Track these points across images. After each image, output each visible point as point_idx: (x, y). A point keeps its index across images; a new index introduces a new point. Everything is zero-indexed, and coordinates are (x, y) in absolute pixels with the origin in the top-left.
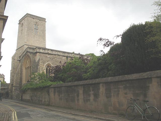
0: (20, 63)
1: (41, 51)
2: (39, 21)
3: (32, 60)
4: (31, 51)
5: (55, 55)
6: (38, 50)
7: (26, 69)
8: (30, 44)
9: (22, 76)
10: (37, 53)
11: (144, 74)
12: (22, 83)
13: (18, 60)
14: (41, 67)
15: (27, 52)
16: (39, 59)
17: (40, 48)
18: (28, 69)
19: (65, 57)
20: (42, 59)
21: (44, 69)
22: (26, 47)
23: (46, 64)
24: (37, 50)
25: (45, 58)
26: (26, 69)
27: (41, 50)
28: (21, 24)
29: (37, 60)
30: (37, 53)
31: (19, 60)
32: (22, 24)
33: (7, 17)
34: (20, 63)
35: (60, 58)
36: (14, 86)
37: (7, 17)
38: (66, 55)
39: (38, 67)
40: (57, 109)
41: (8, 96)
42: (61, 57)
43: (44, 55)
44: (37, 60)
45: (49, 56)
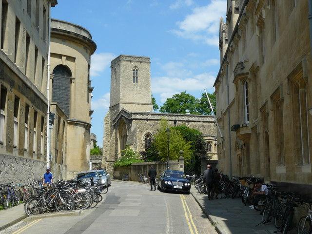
1: (138, 117)
5: (158, 120)
6: (133, 117)
10: (132, 120)
12: (117, 157)
15: (122, 116)
16: (136, 128)
21: (142, 139)
23: (145, 133)
30: (132, 120)
45: (148, 122)
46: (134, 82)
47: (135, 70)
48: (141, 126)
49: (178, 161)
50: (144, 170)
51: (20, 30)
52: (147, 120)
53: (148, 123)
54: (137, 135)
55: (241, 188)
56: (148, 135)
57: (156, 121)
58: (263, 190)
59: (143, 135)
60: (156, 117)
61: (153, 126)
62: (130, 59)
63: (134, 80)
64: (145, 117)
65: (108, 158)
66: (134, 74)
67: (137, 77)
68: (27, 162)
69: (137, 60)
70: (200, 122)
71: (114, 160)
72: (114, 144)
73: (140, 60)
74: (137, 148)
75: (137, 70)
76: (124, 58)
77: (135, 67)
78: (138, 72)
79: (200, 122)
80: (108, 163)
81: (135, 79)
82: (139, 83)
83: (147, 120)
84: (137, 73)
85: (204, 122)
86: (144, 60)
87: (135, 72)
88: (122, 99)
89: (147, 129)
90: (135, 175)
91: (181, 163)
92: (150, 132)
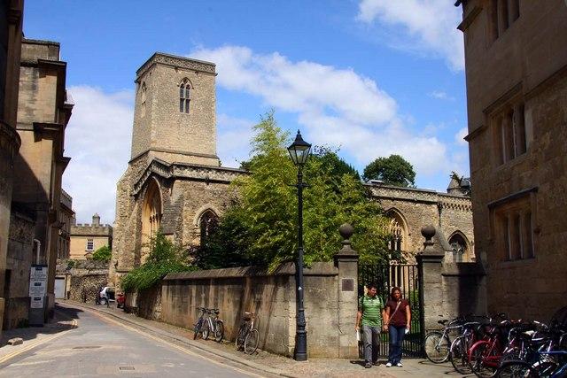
1: (187, 173)
4: (161, 172)
6: (177, 173)
10: (173, 179)
12: (139, 261)
14: (185, 220)
15: (153, 173)
16: (181, 198)
21: (194, 223)
29: (174, 200)
30: (173, 179)
36: (118, 267)
39: (177, 220)
43: (196, 183)
45: (210, 187)
47: (185, 85)
49: (336, 265)
50: (198, 294)
52: (208, 181)
53: (208, 188)
54: (184, 214)
55: (537, 364)
56: (207, 214)
59: (197, 215)
60: (226, 177)
62: (177, 63)
64: (203, 174)
65: (120, 264)
66: (182, 95)
67: (188, 101)
68: (40, 285)
73: (196, 67)
74: (189, 235)
75: (188, 87)
76: (162, 61)
77: (185, 80)
78: (191, 91)
80: (119, 275)
81: (185, 103)
82: (191, 112)
83: (208, 181)
84: (187, 93)
86: (202, 68)
87: (185, 89)
88: (155, 142)
89: (206, 202)
90: (174, 307)
91: (348, 271)
92: (213, 207)
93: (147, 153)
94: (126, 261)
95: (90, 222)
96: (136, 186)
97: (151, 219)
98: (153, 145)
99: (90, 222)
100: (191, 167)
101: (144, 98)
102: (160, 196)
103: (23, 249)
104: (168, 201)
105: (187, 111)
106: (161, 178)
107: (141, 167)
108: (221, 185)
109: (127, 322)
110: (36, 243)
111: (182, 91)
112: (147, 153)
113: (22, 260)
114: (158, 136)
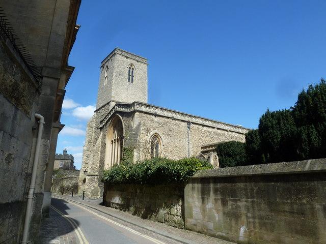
0: (102, 133)
1: (143, 109)
2: (135, 62)
3: (125, 125)
5: (168, 118)
6: (137, 107)
7: (112, 144)
8: (121, 101)
9: (104, 156)
10: (135, 111)
11: (292, 164)
13: (98, 128)
15: (116, 112)
16: (140, 124)
17: (140, 104)
18: (116, 143)
19: (186, 123)
20: (144, 125)
22: (113, 104)
23: (152, 133)
24: (136, 106)
25: (149, 122)
26: (112, 144)
27: (143, 107)
28: (105, 67)
30: (135, 111)
31: (101, 126)
32: (107, 67)
33: (73, 68)
34: (102, 133)
35: (176, 124)
36: (88, 173)
37: (73, 68)
38: (187, 119)
40: (119, 227)
41: (77, 191)
42: (177, 122)
43: (149, 116)
44: (135, 126)
45: (156, 119)
46: (129, 81)
48: (149, 124)
51: (30, 205)
52: (156, 115)
54: (141, 135)
57: (166, 120)
58: (273, 237)
61: (163, 125)
63: (129, 80)
67: (133, 76)
69: (134, 57)
70: (214, 128)
71: (97, 173)
72: (99, 153)
77: (132, 65)
79: (214, 128)
82: (134, 83)
83: (156, 115)
84: (133, 72)
85: (218, 129)
87: (131, 70)
89: (154, 129)
93: (108, 103)
94: (93, 168)
95: (62, 153)
96: (101, 122)
97: (112, 141)
98: (112, 99)
99: (62, 153)
100: (146, 105)
101: (106, 74)
102: (122, 126)
103: (15, 118)
104: (129, 127)
105: (132, 82)
106: (122, 113)
107: (104, 112)
108: (163, 119)
109: (144, 230)
110: (38, 119)
111: (129, 71)
112: (108, 103)
113: (12, 136)
114: (116, 94)
